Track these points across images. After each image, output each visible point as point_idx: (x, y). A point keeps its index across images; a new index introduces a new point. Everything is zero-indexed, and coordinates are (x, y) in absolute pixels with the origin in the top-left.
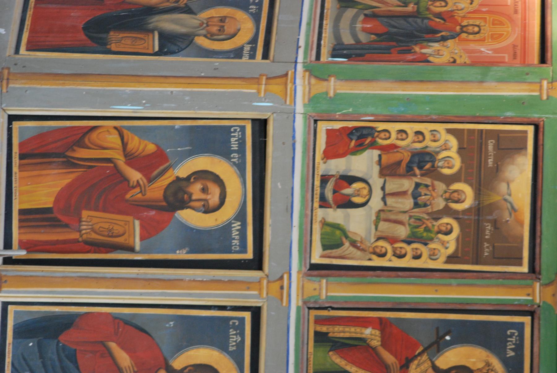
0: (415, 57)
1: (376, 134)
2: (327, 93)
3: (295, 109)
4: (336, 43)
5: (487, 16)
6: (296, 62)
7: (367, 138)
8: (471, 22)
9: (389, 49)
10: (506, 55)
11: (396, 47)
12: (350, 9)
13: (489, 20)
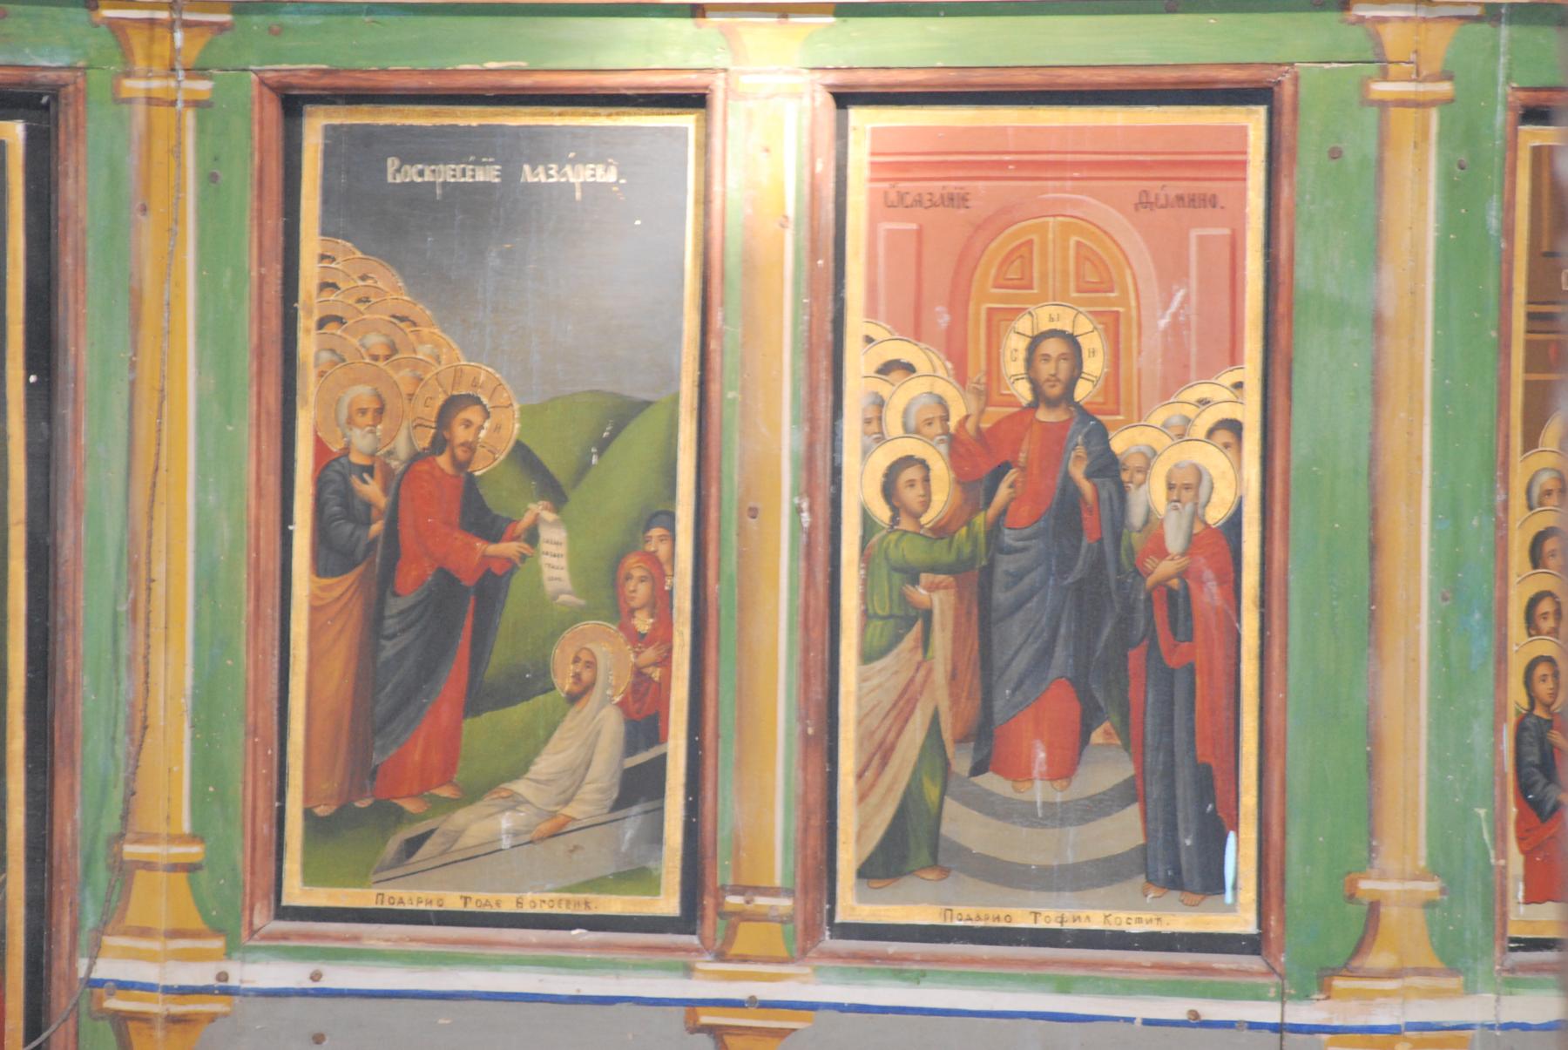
0: (1208, 574)
1: (1539, 712)
2: (1429, 905)
3: (1483, 1025)
4: (1141, 879)
5: (979, 311)
6: (1278, 1028)
7: (1552, 746)
8: (1014, 366)
9: (1167, 677)
10: (1194, 234)
11: (1154, 645)
12: (946, 829)
13: (1002, 299)
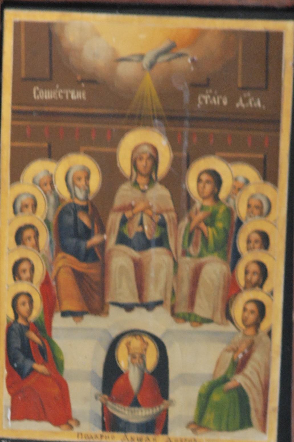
1: (21, 321)
7: (29, 340)
